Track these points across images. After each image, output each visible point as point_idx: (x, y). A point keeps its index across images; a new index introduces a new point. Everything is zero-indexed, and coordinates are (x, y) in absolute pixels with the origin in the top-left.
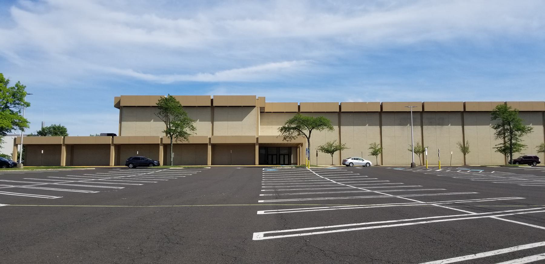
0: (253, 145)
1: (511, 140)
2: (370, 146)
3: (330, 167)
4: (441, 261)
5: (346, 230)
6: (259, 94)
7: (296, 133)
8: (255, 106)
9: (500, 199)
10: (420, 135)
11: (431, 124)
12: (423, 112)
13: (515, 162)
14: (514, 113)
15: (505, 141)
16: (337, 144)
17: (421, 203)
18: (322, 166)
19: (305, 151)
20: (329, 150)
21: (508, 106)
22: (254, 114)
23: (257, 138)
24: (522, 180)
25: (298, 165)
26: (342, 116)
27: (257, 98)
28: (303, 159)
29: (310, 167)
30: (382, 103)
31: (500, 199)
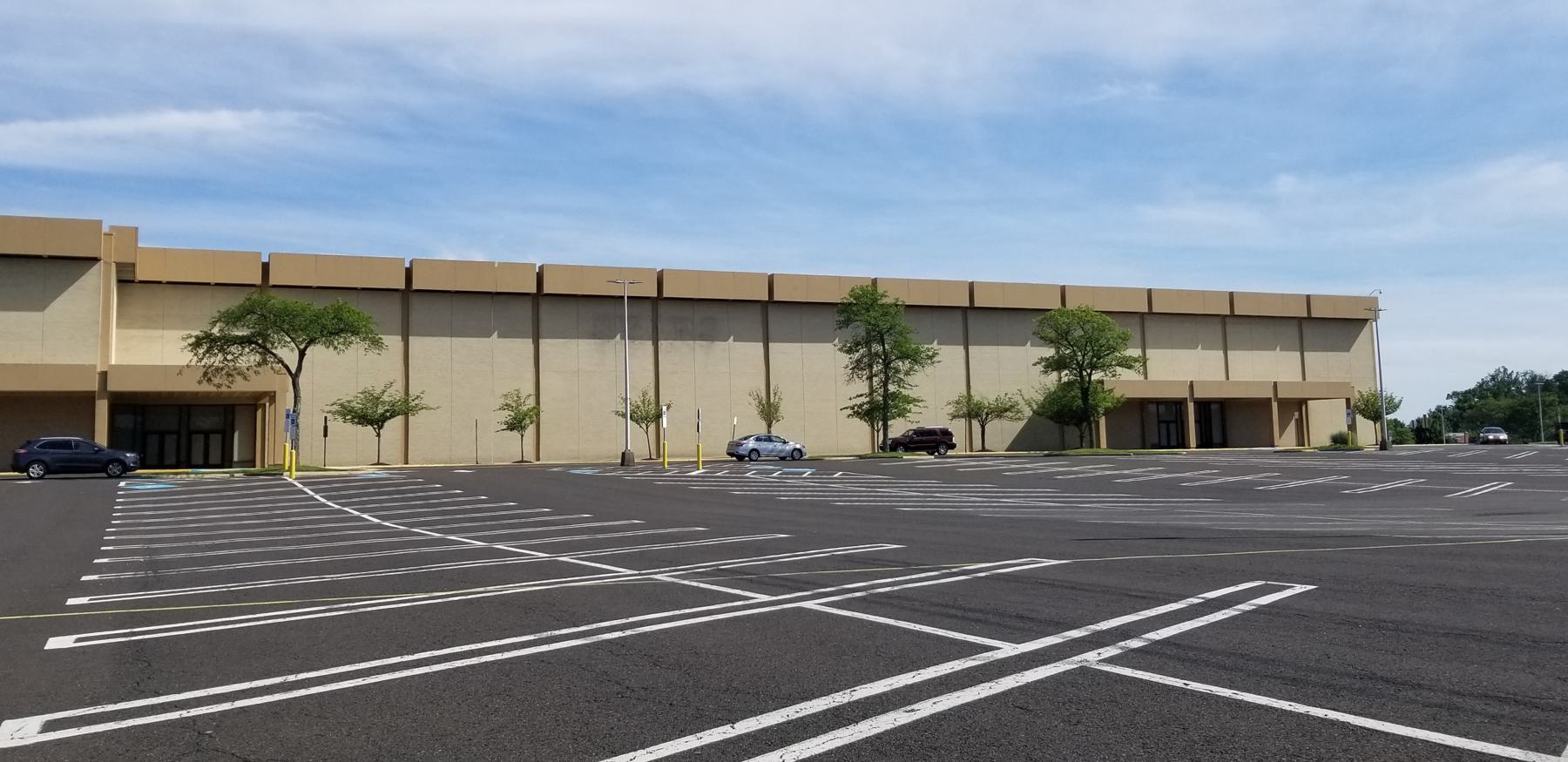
0: (88, 399)
1: (885, 384)
2: (502, 401)
3: (370, 471)
4: (631, 755)
5: (359, 682)
6: (112, 217)
7: (248, 358)
8: (96, 260)
9: (840, 551)
10: (651, 367)
11: (681, 335)
12: (659, 300)
13: (896, 445)
14: (892, 310)
15: (871, 386)
16: (395, 394)
17: (625, 574)
18: (340, 467)
19: (282, 421)
20: (370, 416)
21: (880, 291)
22: (95, 286)
23: (104, 375)
24: (905, 496)
25: (258, 468)
26: (415, 302)
27: (105, 229)
28: (278, 448)
29: (295, 474)
30: (541, 268)
31: (840, 551)
